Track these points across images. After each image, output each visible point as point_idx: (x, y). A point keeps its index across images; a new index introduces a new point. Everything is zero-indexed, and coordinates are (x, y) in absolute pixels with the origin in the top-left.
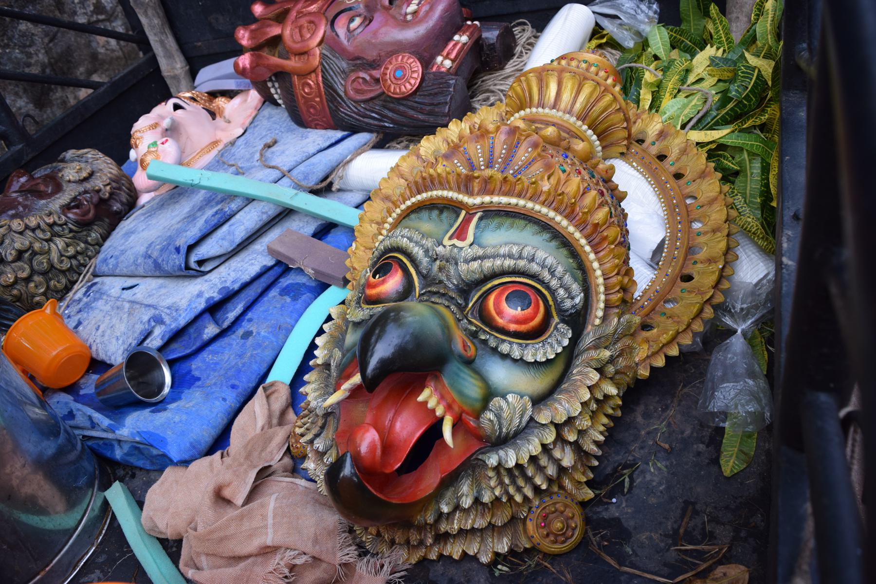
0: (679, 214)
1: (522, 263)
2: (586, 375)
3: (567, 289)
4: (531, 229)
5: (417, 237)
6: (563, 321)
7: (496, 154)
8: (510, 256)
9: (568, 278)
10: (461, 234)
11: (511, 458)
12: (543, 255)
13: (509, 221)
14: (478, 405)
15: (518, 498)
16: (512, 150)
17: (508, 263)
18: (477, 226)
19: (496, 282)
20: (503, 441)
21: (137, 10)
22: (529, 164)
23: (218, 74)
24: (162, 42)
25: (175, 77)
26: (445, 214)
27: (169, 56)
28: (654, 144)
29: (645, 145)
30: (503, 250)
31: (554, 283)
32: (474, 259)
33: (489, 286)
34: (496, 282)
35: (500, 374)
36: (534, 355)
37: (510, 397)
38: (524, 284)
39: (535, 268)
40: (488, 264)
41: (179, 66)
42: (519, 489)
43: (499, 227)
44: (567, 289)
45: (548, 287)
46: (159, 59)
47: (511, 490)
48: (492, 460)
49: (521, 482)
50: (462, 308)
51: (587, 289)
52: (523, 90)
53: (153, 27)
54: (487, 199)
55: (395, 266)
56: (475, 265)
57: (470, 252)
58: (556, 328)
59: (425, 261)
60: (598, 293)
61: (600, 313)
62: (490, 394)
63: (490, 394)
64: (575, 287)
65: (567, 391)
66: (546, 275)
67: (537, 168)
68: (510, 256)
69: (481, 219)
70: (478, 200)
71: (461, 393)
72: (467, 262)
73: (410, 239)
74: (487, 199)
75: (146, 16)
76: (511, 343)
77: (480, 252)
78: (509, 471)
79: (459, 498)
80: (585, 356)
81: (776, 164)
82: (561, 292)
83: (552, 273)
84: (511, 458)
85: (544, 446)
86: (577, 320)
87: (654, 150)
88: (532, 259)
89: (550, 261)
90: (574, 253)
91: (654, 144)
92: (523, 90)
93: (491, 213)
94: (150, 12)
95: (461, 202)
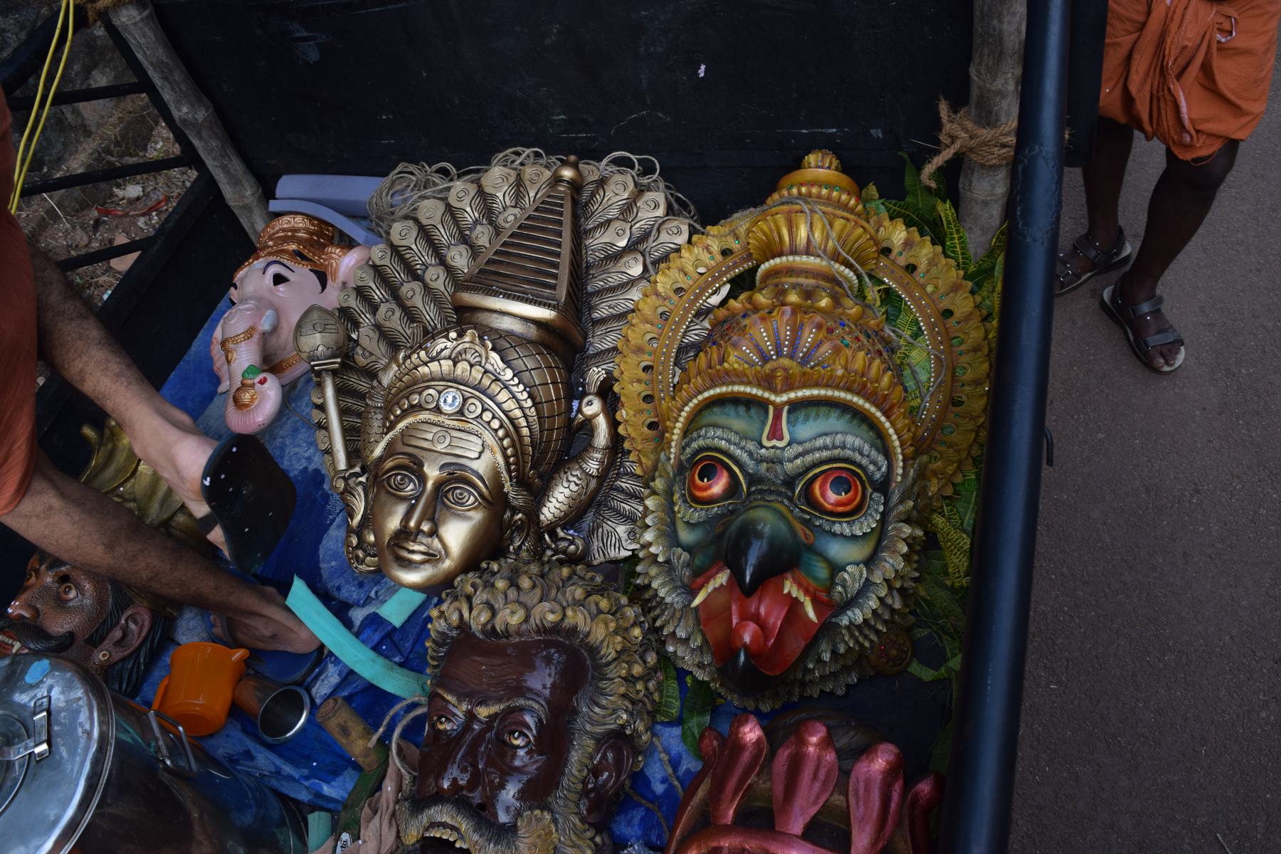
0: (938, 333)
1: (836, 452)
2: (900, 530)
3: (874, 463)
4: (835, 414)
5: (734, 438)
6: (875, 490)
7: (782, 337)
8: (826, 448)
9: (873, 453)
10: (776, 433)
11: (857, 615)
12: (854, 441)
13: (813, 411)
14: (828, 583)
15: (867, 644)
16: (797, 331)
17: (825, 454)
18: (788, 422)
19: (817, 471)
20: (849, 604)
21: (187, 132)
22: (817, 345)
23: (318, 194)
24: (224, 168)
25: (246, 208)
26: (753, 411)
27: (235, 182)
28: (901, 254)
29: (892, 256)
30: (819, 442)
31: (864, 462)
32: (796, 457)
33: (810, 475)
34: (817, 471)
35: (836, 550)
36: (861, 529)
37: (849, 568)
38: (846, 474)
39: (848, 453)
40: (809, 459)
41: (249, 193)
42: (866, 637)
43: (807, 419)
44: (874, 463)
45: (859, 466)
46: (221, 186)
47: (861, 639)
48: (845, 621)
49: (866, 631)
50: (791, 499)
51: (887, 452)
52: (770, 229)
53: (210, 151)
54: (792, 395)
55: (719, 467)
56: (798, 461)
57: (789, 453)
58: (871, 499)
59: (750, 465)
60: (895, 454)
61: (900, 471)
62: (836, 569)
63: (836, 569)
64: (881, 459)
65: (887, 548)
66: (858, 457)
67: (826, 349)
68: (826, 448)
69: (789, 412)
70: (784, 398)
71: (815, 578)
72: (790, 461)
73: (728, 441)
74: (792, 395)
75: (200, 138)
76: (840, 523)
77: (800, 449)
78: (859, 627)
79: (819, 655)
80: (895, 513)
81: (1015, 111)
82: (872, 467)
83: (861, 453)
84: (857, 615)
85: (880, 599)
86: (883, 486)
87: (902, 261)
88: (843, 447)
89: (858, 442)
90: (873, 425)
91: (901, 254)
92: (770, 229)
93: (795, 406)
94: (205, 134)
95: (767, 399)
